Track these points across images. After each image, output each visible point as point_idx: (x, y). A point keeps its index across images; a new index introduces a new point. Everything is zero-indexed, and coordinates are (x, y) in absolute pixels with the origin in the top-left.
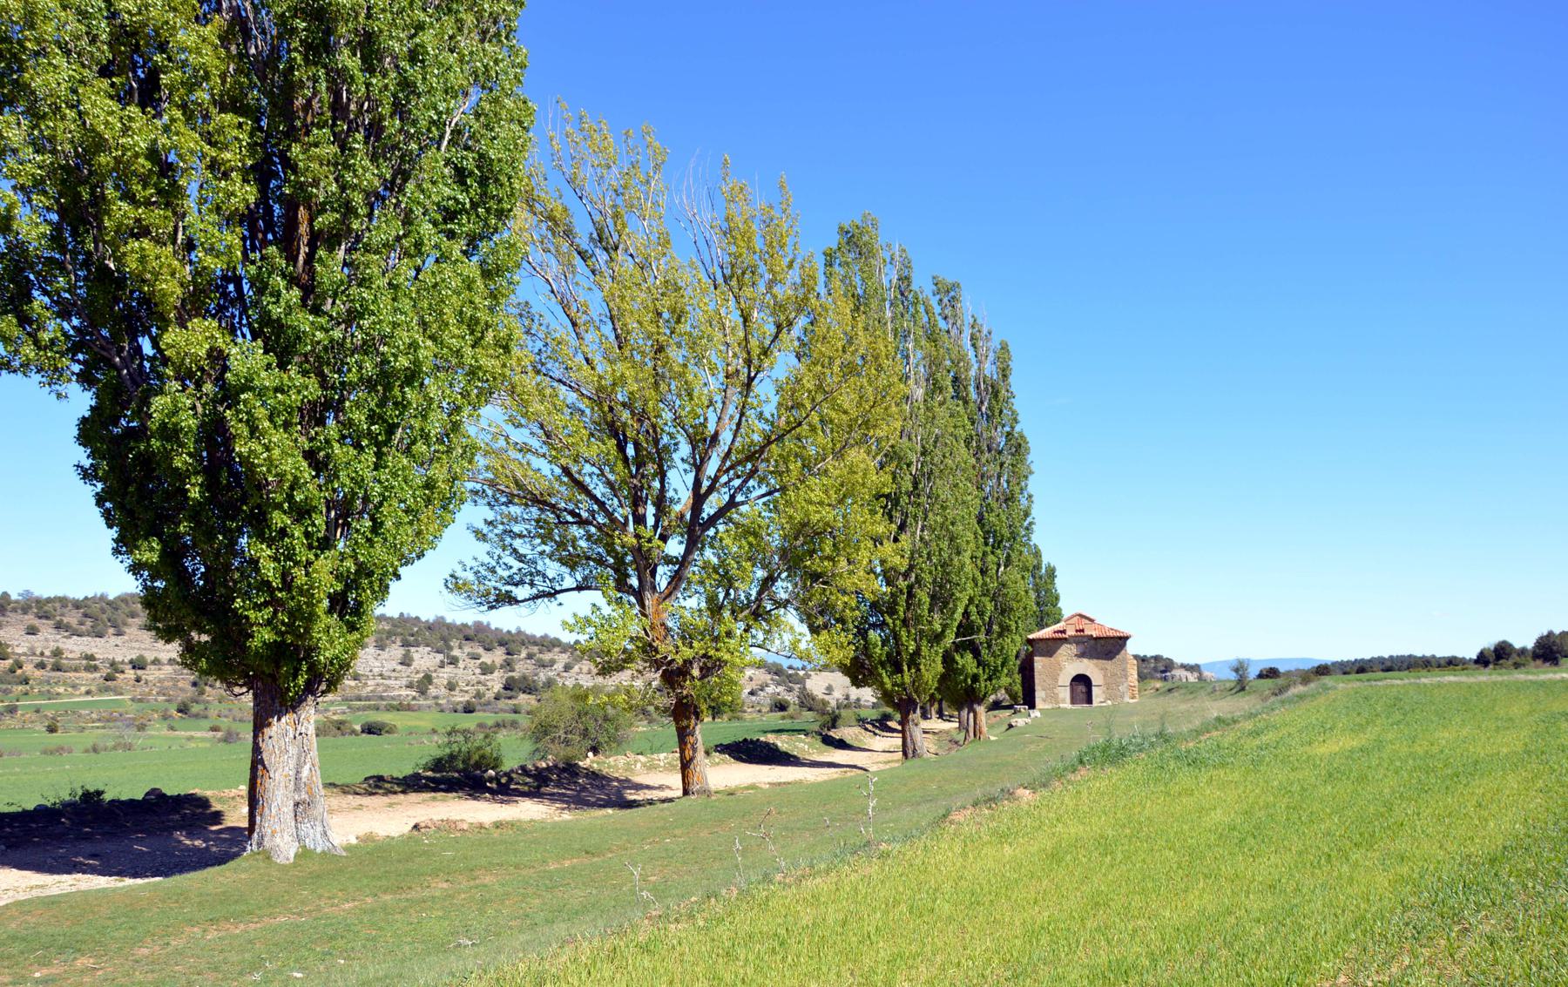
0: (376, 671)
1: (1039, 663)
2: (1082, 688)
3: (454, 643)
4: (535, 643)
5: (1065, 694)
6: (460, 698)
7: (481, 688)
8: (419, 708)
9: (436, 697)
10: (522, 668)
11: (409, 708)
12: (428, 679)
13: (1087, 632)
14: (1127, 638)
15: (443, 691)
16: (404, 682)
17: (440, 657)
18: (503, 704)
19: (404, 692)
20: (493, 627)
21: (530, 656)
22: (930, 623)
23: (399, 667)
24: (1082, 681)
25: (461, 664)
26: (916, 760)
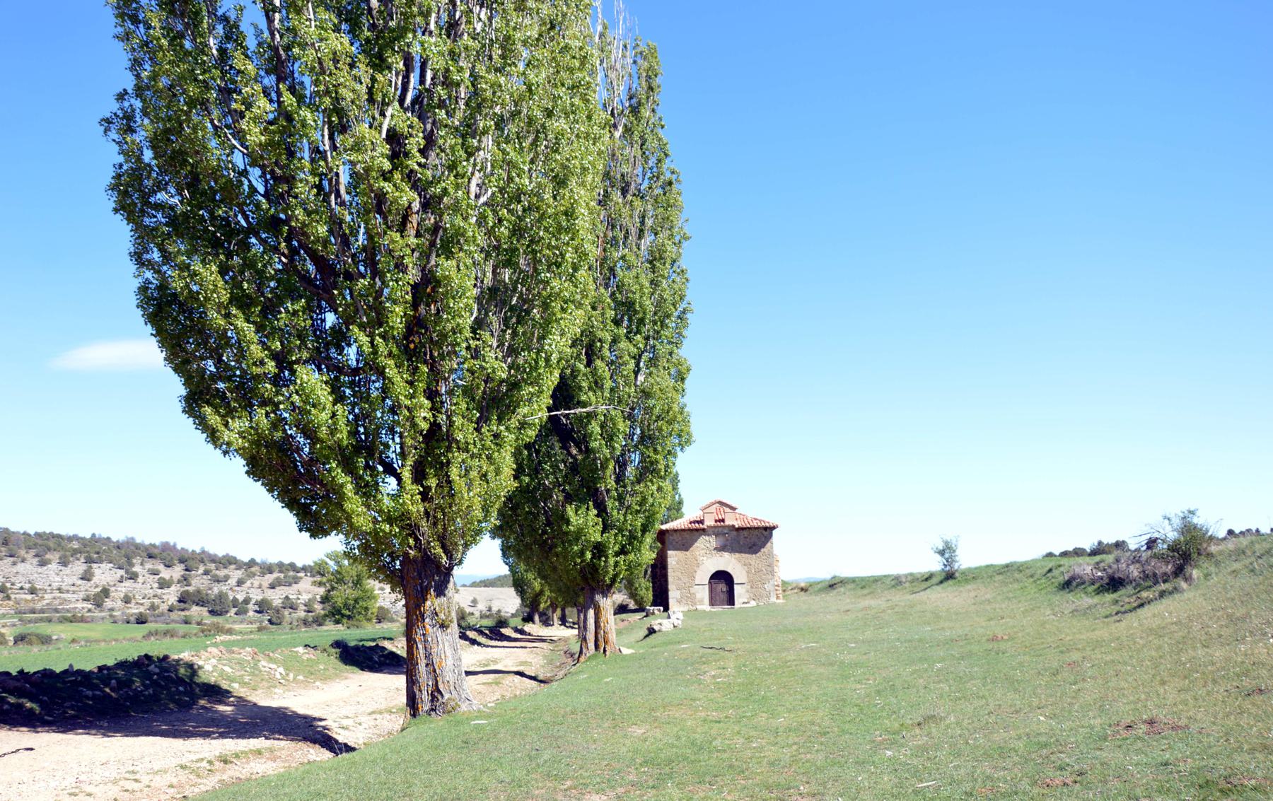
0: (55, 585)
1: (673, 557)
2: (722, 587)
3: (136, 561)
4: (213, 561)
5: (703, 593)
6: (134, 610)
7: (156, 601)
8: (92, 620)
9: (112, 610)
10: (199, 582)
11: (83, 620)
12: (105, 592)
13: (728, 522)
14: (774, 528)
15: (119, 603)
16: (82, 595)
17: (122, 572)
18: (176, 615)
19: (80, 605)
20: (179, 547)
21: (206, 573)
22: (476, 354)
23: (80, 582)
24: (723, 578)
25: (140, 579)
26: (438, 721)
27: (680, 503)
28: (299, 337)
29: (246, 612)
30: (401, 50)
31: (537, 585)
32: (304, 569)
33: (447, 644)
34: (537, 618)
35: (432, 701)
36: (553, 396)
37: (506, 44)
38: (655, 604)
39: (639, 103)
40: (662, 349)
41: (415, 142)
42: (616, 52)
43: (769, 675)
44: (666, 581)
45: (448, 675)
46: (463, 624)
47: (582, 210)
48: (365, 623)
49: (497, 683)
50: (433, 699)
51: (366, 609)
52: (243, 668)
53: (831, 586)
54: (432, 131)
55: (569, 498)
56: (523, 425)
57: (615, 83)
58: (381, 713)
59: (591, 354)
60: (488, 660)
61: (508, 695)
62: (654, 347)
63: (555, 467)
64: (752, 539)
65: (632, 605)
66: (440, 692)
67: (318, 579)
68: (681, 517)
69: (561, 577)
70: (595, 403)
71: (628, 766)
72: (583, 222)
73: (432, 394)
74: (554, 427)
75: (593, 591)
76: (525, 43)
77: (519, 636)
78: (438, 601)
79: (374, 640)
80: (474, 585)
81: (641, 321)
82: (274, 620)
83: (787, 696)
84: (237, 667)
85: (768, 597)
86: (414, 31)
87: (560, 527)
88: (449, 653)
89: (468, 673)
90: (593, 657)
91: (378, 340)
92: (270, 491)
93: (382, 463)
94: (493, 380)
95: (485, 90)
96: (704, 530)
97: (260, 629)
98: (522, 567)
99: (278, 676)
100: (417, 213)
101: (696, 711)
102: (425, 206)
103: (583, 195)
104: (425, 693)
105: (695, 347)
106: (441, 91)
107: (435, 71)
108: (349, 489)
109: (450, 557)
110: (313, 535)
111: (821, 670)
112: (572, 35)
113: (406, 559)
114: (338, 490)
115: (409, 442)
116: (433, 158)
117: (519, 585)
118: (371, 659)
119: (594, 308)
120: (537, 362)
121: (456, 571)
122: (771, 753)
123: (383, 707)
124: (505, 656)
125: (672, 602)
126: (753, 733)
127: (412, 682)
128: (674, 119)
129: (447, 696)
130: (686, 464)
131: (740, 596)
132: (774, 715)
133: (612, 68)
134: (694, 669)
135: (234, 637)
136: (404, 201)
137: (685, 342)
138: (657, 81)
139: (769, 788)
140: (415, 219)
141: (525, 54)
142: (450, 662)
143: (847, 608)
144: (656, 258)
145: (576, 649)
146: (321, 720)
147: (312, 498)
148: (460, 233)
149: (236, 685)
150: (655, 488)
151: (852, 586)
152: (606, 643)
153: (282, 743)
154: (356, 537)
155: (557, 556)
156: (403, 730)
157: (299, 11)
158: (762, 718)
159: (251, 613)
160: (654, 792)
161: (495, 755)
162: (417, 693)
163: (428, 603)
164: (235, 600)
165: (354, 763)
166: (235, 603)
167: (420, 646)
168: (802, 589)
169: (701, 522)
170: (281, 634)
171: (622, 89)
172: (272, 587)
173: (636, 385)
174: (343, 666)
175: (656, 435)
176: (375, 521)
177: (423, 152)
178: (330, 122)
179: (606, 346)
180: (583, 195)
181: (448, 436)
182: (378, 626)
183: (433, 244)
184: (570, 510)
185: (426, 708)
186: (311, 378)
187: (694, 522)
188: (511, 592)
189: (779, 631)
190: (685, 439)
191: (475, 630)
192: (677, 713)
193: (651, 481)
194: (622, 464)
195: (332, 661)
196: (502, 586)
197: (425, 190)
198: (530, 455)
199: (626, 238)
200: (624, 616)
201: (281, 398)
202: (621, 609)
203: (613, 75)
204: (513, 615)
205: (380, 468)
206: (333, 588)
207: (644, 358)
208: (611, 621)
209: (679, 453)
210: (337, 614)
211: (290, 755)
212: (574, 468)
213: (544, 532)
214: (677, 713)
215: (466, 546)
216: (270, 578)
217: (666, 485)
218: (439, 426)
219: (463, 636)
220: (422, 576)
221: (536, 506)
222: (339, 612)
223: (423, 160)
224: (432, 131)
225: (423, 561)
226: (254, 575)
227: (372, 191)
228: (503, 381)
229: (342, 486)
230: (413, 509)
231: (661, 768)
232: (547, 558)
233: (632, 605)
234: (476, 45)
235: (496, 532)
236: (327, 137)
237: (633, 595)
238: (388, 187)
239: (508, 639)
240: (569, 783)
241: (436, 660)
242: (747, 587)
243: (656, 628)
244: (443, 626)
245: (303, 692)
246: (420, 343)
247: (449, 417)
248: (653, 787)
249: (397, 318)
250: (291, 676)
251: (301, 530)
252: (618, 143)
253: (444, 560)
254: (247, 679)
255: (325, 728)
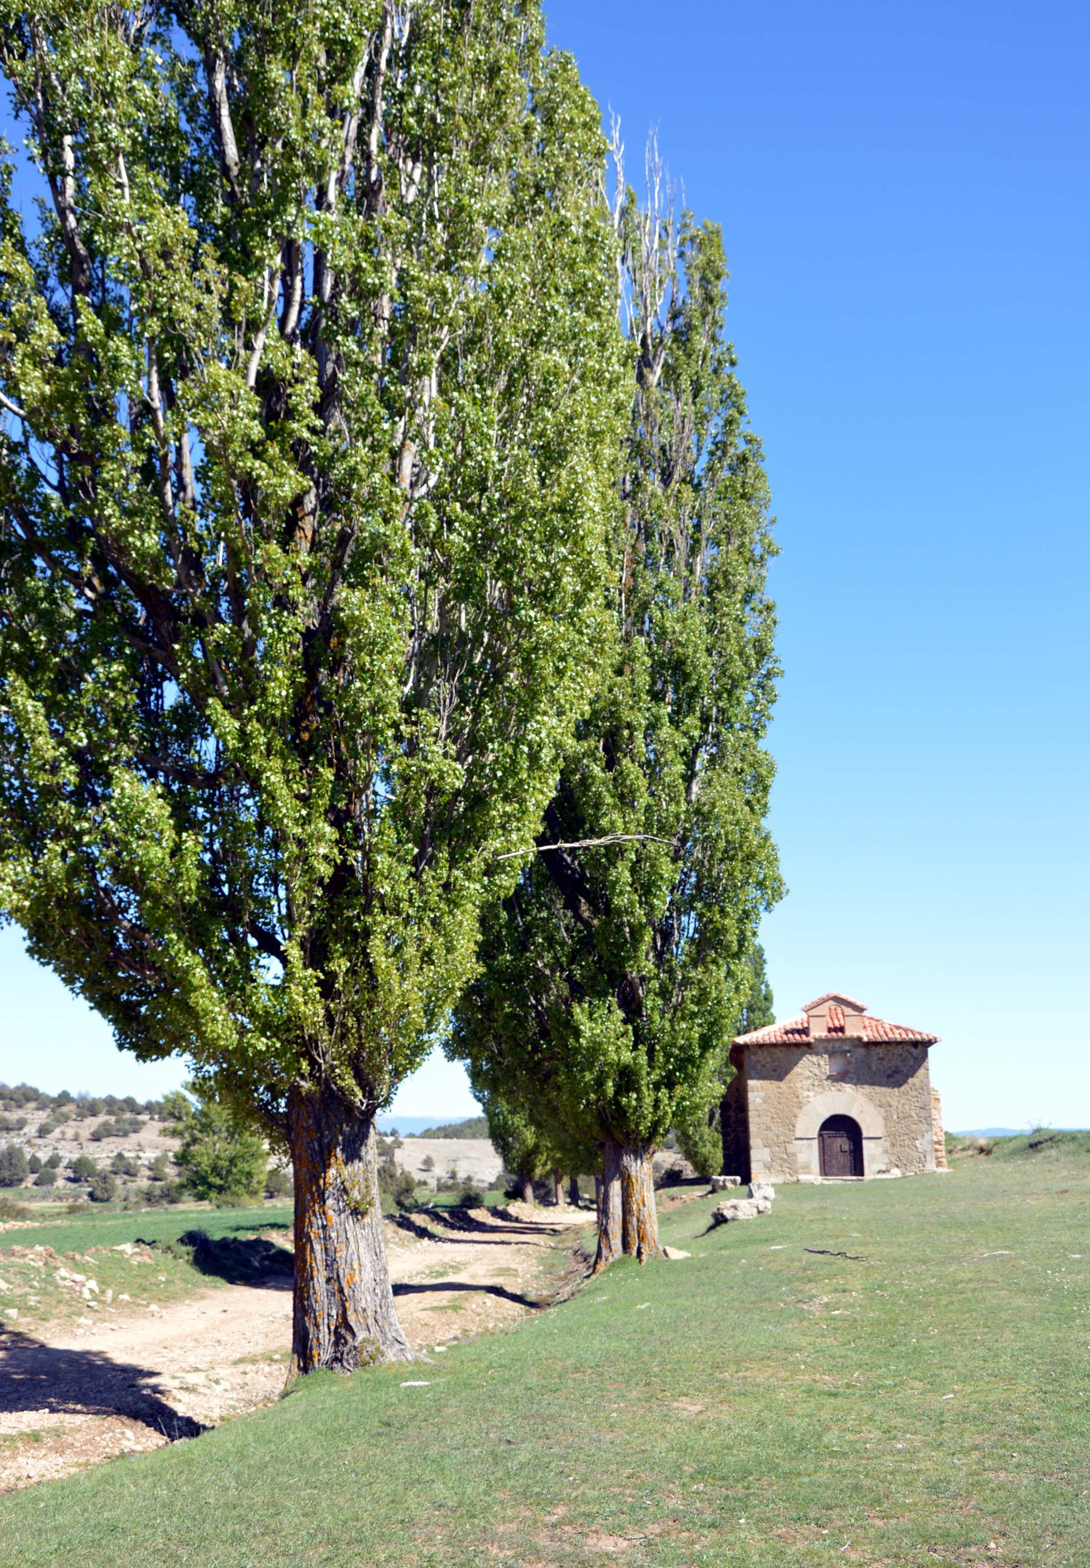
1: (758, 1091)
2: (842, 1143)
5: (809, 1154)
13: (851, 1032)
14: (930, 1043)
24: (842, 1129)
26: (346, 1379)
27: (768, 998)
28: (117, 723)
29: (52, 1180)
30: (277, 236)
31: (529, 1136)
32: (149, 1108)
33: (362, 1244)
34: (529, 1192)
35: (336, 1344)
36: (549, 816)
37: (457, 217)
38: (727, 1171)
39: (690, 327)
40: (730, 739)
41: (306, 393)
42: (649, 242)
43: (925, 1306)
44: (746, 1131)
45: (365, 1297)
46: (407, 1202)
47: (591, 502)
48: (246, 1198)
49: (456, 1308)
50: (339, 1340)
51: (249, 1175)
52: (27, 1281)
53: (1034, 1146)
54: (334, 374)
55: (578, 991)
56: (491, 870)
57: (647, 293)
58: (254, 1361)
59: (613, 747)
60: (445, 1265)
61: (474, 1329)
62: (716, 736)
63: (551, 941)
64: (895, 1061)
65: (689, 1172)
66: (349, 1328)
67: (171, 1124)
68: (771, 1021)
69: (568, 1126)
70: (620, 827)
71: (669, 1480)
72: (593, 527)
73: (338, 818)
74: (552, 873)
75: (619, 1149)
76: (488, 218)
77: (499, 1223)
78: (347, 1171)
79: (253, 1228)
80: (428, 1134)
81: (694, 694)
82: (98, 1193)
83: (958, 1349)
84: (19, 1280)
85: (922, 1161)
86: (299, 202)
87: (564, 1039)
88: (366, 1259)
89: (400, 1289)
90: (620, 1262)
91: (254, 726)
92: (69, 981)
93: (257, 933)
94: (441, 792)
95: (419, 300)
96: (808, 1045)
97: (73, 1210)
98: (504, 1106)
99: (87, 1295)
100: (313, 512)
101: (795, 1372)
102: (327, 505)
103: (592, 480)
104: (324, 1329)
105: (787, 738)
106: (349, 308)
107: (338, 272)
108: (200, 974)
109: (369, 1090)
110: (142, 1056)
111: (1019, 1301)
112: (576, 206)
113: (295, 1096)
114: (180, 979)
115: (300, 897)
116: (337, 419)
117: (500, 1136)
118: (247, 1263)
119: (619, 672)
120: (514, 762)
121: (382, 1119)
122: (930, 1463)
123: (259, 1350)
124: (473, 1258)
125: (756, 1168)
126: (898, 1421)
127: (302, 1310)
128: (746, 333)
129: (361, 1335)
130: (771, 931)
131: (873, 1159)
132: (935, 1385)
133: (644, 267)
134: (793, 1292)
135: (28, 1224)
136: (287, 492)
137: (771, 726)
138: (718, 288)
139: (928, 1540)
140: (308, 524)
141: (491, 239)
142: (368, 1275)
143: (1065, 1185)
144: (717, 584)
145: (592, 1248)
146: (152, 1374)
147: (142, 993)
148: (379, 543)
149: (13, 1312)
150: (723, 974)
151: (1072, 1147)
152: (641, 1239)
153: (79, 1419)
154: (213, 1057)
155: (559, 1088)
156: (285, 1395)
157: (102, 171)
158: (913, 1392)
159: (60, 1183)
160: (712, 1536)
161: (434, 1451)
162: (311, 1329)
163: (332, 1172)
164: (35, 1160)
165: (189, 1463)
166: (34, 1165)
167: (317, 1247)
168: (982, 1150)
169: (805, 1031)
170: (107, 1219)
171: (661, 302)
172: (96, 1138)
173: (689, 802)
174: (199, 1277)
175: (722, 883)
176: (242, 1031)
177: (320, 409)
178: (161, 361)
179: (639, 735)
180: (592, 480)
181: (366, 887)
182: (268, 1204)
183: (337, 564)
184: (579, 1012)
185: (326, 1357)
186: (136, 790)
187: (793, 1031)
188: (486, 1146)
189: (942, 1225)
190: (772, 890)
191: (427, 1212)
192: (760, 1375)
193: (714, 962)
194: (665, 933)
195: (181, 1266)
196: (474, 1136)
197: (323, 473)
198: (512, 918)
199: (669, 554)
200: (674, 1191)
201: (86, 825)
202: (671, 1179)
203: (645, 277)
204: (492, 1187)
205: (253, 942)
206: (195, 1140)
207: (703, 757)
208: (649, 1200)
209: (764, 915)
210: (201, 1183)
211: (89, 1442)
212: (586, 943)
213: (536, 1049)
214: (760, 1375)
215: (398, 1074)
216: (92, 1123)
217: (743, 969)
218: (351, 870)
219: (405, 1224)
220: (325, 1123)
221: (523, 1005)
222: (204, 1180)
223: (319, 423)
224: (334, 374)
225: (323, 1100)
226: (66, 1118)
227: (233, 475)
228: (458, 793)
229: (187, 971)
230: (306, 1010)
231: (729, 1485)
232: (541, 1092)
233: (689, 1172)
234: (406, 225)
235: (456, 1047)
236: (155, 386)
237: (690, 1155)
238: (260, 468)
239: (481, 1227)
240: (561, 1511)
241: (344, 1271)
242: (885, 1143)
243: (728, 1214)
244: (357, 1212)
245: (126, 1323)
246: (317, 729)
247: (366, 855)
248: (713, 1525)
249: (280, 687)
250: (110, 1293)
251: (121, 1047)
252: (656, 393)
253: (359, 1097)
254: (32, 1300)
255: (155, 1389)
